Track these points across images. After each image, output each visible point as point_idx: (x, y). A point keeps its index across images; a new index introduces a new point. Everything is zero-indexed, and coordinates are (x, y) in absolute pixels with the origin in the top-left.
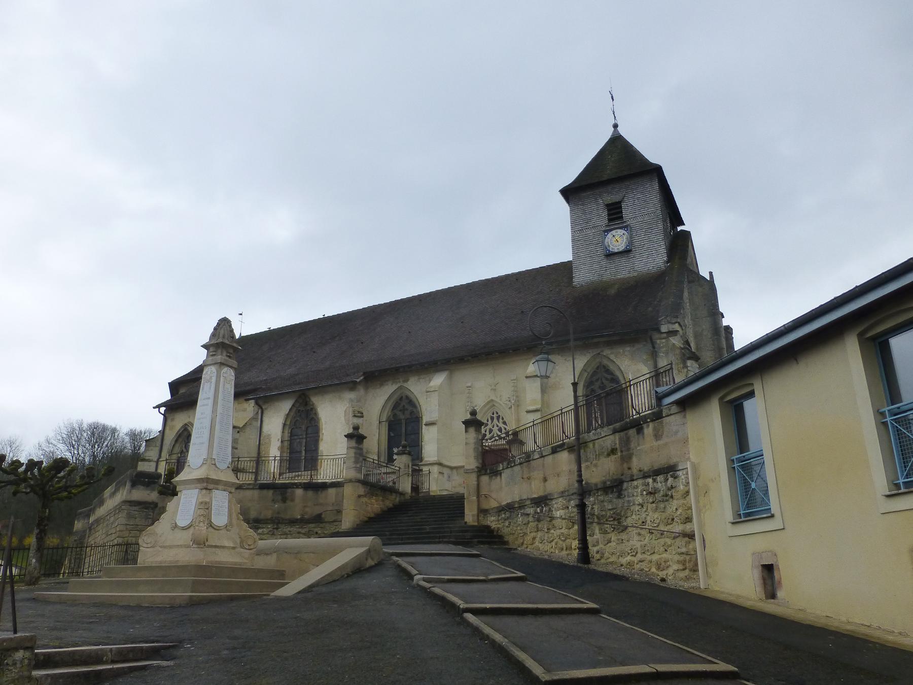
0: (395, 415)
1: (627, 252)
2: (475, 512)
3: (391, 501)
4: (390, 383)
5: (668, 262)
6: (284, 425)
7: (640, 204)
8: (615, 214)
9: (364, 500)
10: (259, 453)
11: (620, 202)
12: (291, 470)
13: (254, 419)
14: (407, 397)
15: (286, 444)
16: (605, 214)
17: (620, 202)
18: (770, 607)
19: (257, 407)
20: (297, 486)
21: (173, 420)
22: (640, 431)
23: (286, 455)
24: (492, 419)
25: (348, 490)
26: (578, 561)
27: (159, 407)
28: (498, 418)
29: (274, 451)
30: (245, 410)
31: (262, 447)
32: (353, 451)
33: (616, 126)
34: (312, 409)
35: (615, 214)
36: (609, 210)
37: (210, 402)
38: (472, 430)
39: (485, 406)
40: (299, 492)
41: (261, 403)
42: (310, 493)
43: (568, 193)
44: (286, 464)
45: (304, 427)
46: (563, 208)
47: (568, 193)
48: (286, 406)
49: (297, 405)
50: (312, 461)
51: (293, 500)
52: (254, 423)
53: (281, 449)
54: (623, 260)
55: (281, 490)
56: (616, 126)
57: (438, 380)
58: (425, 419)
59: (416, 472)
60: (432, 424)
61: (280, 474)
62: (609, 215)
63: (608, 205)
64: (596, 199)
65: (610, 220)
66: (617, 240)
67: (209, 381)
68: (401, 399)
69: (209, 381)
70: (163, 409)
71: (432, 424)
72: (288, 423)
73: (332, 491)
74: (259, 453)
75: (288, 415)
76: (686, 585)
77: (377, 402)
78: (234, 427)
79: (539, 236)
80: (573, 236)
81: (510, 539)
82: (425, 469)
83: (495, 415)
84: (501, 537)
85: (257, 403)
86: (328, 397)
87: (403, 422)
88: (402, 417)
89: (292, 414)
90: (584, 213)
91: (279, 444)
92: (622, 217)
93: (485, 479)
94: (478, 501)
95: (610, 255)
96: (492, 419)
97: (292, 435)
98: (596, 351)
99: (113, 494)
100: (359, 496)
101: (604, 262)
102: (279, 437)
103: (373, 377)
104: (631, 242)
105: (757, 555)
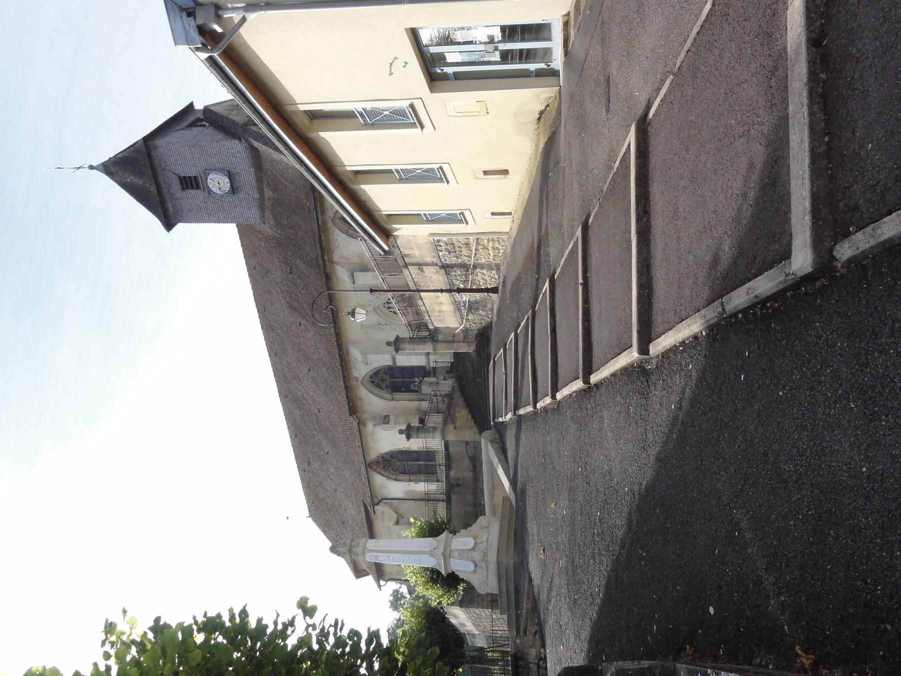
0: (387, 387)
1: (230, 175)
2: (465, 344)
3: (458, 399)
4: (358, 392)
5: (240, 140)
6: (396, 480)
7: (179, 156)
8: (191, 183)
9: (458, 424)
10: (421, 500)
11: (180, 178)
12: (434, 473)
13: (391, 506)
14: (371, 377)
15: (413, 477)
16: (192, 192)
17: (180, 178)
18: (518, 215)
19: (381, 504)
20: (447, 476)
21: (391, 573)
22: (407, 256)
23: (422, 477)
24: (389, 308)
25: (451, 437)
26: (490, 429)
27: (380, 586)
28: (388, 303)
29: (421, 487)
30: (383, 513)
31: (416, 497)
32: (420, 434)
33: (91, 167)
34: (382, 457)
35: (191, 183)
36: (188, 188)
37: (391, 555)
38: (402, 346)
39: (378, 314)
40: (452, 474)
41: (376, 501)
42: (454, 465)
43: (169, 225)
44: (431, 477)
45: (398, 463)
46: (180, 227)
47: (169, 225)
48: (379, 479)
49: (378, 470)
50: (429, 455)
51: (459, 479)
52: (395, 505)
53: (416, 481)
54: (238, 178)
55: (452, 487)
56: (91, 167)
57: (355, 353)
58: (390, 363)
59: (434, 372)
60: (394, 359)
61: (438, 481)
62: (192, 188)
63: (183, 189)
64: (177, 199)
65: (198, 187)
66: (218, 183)
67: (376, 557)
68: (373, 382)
69: (376, 557)
70: (382, 583)
71: (394, 359)
72: (394, 477)
73: (452, 449)
74: (421, 500)
75: (388, 478)
76: (509, 244)
77: (373, 402)
78: (397, 523)
79: (214, 252)
80: (214, 222)
81: (484, 323)
82: (432, 365)
83: (386, 305)
84: (484, 328)
85: (378, 504)
86: (371, 445)
87: (392, 380)
88: (388, 382)
89: (386, 474)
90: (190, 210)
91: (412, 484)
92: (195, 178)
93: (440, 337)
94: (458, 342)
95: (234, 190)
96: (389, 308)
97: (403, 473)
98: (330, 224)
99: (456, 617)
100: (455, 428)
101: (241, 195)
102: (406, 483)
103: (353, 409)
104: (221, 170)
105: (490, 34)
